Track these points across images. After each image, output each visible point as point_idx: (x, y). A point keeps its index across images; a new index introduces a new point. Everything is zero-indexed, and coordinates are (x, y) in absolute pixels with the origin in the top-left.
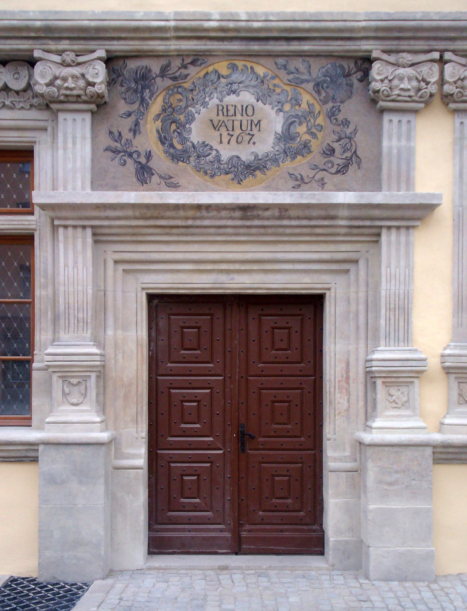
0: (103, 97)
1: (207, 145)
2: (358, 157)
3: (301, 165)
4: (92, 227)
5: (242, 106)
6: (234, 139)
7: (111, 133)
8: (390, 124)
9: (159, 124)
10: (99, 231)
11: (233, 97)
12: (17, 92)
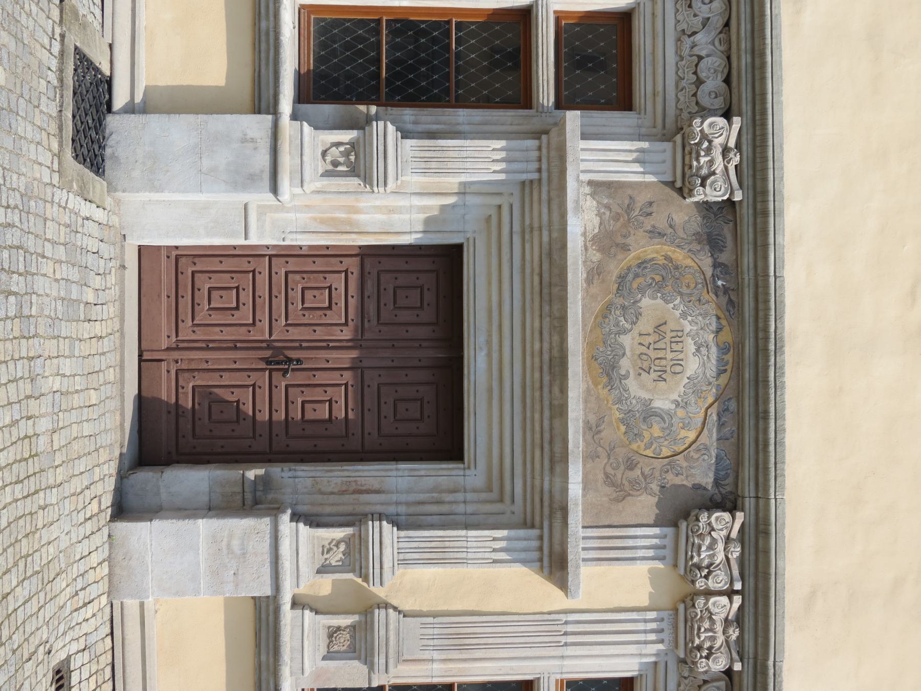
0: (691, 196)
1: (637, 318)
2: (624, 499)
3: (614, 433)
4: (540, 180)
5: (682, 360)
6: (643, 349)
7: (651, 204)
8: (649, 536)
9: (662, 261)
10: (535, 185)
11: (693, 348)
12: (695, 95)
